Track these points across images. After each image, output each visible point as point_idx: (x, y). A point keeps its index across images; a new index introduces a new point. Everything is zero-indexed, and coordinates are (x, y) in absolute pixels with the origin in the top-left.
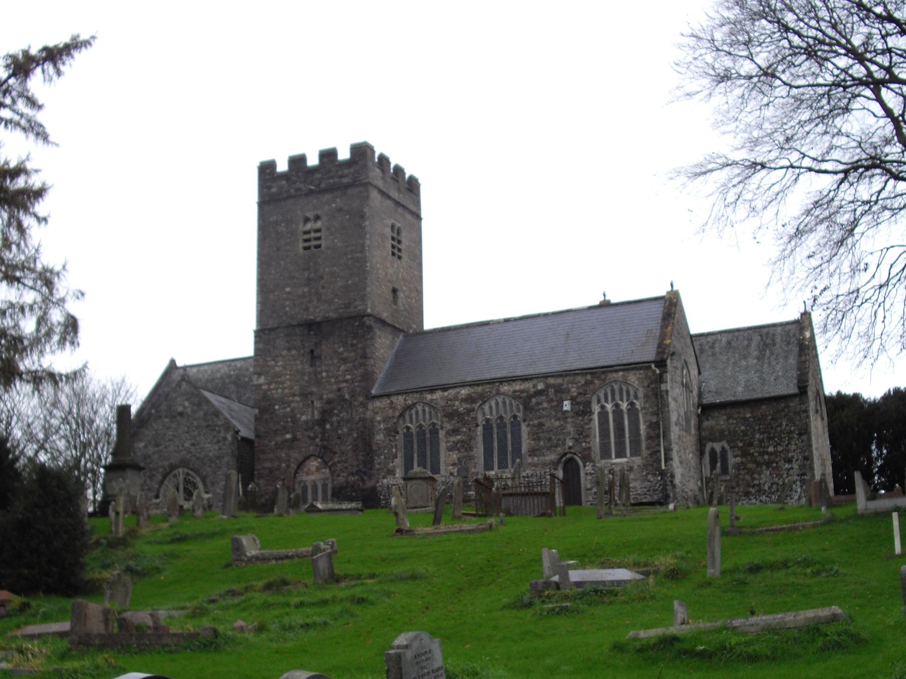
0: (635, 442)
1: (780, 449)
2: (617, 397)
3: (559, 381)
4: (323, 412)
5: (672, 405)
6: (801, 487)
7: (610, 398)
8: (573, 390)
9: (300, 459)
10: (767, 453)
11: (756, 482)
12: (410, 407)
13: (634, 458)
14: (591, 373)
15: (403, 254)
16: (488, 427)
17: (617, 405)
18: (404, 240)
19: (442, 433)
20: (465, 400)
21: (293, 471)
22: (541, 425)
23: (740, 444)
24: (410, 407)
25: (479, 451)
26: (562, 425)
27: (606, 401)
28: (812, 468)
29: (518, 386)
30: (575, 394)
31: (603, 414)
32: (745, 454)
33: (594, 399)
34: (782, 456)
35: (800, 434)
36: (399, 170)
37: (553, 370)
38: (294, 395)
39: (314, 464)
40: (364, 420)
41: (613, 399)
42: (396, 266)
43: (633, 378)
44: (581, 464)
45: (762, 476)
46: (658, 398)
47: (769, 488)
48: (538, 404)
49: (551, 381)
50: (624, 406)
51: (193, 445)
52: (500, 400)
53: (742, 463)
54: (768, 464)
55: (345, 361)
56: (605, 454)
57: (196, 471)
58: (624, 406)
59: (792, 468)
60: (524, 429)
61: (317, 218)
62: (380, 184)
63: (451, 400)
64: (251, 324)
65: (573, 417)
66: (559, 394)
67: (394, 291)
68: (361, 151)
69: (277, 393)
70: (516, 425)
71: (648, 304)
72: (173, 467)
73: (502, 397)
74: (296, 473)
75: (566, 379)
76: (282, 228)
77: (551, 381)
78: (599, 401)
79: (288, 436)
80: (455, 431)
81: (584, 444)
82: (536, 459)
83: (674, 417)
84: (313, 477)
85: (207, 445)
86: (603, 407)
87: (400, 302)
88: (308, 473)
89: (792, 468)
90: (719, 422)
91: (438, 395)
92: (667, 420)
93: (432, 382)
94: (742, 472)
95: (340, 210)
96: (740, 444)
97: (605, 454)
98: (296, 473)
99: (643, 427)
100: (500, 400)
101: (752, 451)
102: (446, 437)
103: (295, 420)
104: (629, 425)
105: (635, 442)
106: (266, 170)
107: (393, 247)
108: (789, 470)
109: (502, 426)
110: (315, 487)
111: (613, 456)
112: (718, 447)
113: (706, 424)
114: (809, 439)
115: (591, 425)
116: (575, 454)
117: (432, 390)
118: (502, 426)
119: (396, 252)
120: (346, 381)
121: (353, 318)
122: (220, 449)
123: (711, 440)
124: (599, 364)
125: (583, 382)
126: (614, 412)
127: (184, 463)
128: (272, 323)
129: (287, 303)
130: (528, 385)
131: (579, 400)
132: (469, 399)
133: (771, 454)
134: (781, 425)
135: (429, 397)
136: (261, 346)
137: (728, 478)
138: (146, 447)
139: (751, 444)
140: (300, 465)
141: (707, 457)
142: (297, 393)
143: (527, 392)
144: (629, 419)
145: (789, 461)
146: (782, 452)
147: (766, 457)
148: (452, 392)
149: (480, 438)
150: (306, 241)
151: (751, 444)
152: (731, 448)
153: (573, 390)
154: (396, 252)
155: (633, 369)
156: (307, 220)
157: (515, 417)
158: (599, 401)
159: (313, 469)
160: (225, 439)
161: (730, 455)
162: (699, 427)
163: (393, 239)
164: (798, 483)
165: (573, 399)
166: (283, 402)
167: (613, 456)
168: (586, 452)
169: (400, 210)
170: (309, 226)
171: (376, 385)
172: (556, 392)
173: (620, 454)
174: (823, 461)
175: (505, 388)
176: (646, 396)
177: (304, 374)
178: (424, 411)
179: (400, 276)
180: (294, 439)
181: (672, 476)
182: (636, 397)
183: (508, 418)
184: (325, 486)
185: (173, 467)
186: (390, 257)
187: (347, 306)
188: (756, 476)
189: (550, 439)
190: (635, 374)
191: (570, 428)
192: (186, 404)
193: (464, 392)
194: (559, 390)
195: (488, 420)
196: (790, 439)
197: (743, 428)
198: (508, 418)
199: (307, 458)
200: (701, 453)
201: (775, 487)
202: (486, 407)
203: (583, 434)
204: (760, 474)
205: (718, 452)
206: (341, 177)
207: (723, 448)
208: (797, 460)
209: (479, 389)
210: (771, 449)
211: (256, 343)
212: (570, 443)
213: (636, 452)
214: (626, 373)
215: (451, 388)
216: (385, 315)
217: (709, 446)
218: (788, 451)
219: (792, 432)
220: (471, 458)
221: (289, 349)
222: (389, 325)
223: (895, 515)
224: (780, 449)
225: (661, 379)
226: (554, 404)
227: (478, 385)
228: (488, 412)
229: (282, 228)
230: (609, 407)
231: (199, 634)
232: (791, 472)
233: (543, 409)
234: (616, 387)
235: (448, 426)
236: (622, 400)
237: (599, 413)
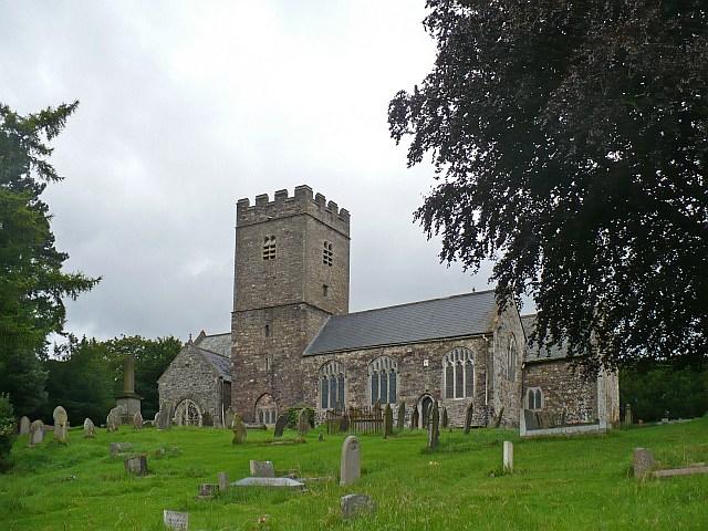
0: (470, 387)
3: (422, 346)
4: (273, 366)
5: (496, 362)
16: (375, 377)
17: (459, 363)
22: (409, 375)
24: (327, 363)
29: (395, 350)
31: (450, 369)
32: (553, 395)
36: (333, 205)
39: (267, 398)
43: (470, 344)
46: (486, 357)
50: (463, 363)
52: (383, 358)
55: (287, 332)
56: (450, 394)
57: (197, 402)
58: (463, 363)
61: (273, 238)
62: (316, 215)
64: (229, 306)
67: (325, 287)
68: (303, 191)
69: (245, 354)
70: (393, 375)
71: (464, 299)
72: (183, 399)
76: (250, 245)
77: (417, 346)
80: (354, 379)
83: (497, 371)
86: (450, 364)
87: (329, 295)
90: (537, 373)
91: (344, 355)
92: (491, 375)
93: (334, 347)
95: (287, 233)
97: (450, 394)
100: (383, 358)
103: (256, 371)
105: (470, 387)
106: (242, 205)
107: (325, 257)
110: (268, 414)
112: (534, 390)
114: (596, 385)
117: (341, 352)
119: (328, 261)
123: (530, 386)
127: (190, 397)
130: (402, 350)
132: (364, 358)
141: (527, 397)
148: (353, 353)
149: (370, 384)
150: (265, 253)
154: (328, 261)
156: (267, 239)
162: (523, 377)
165: (430, 359)
169: (332, 232)
170: (269, 243)
171: (307, 349)
174: (609, 400)
176: (478, 356)
180: (255, 383)
181: (493, 410)
183: (388, 371)
184: (274, 413)
185: (183, 399)
187: (290, 296)
194: (422, 353)
198: (388, 371)
202: (374, 363)
203: (436, 382)
209: (371, 351)
210: (570, 391)
212: (427, 387)
213: (470, 393)
216: (316, 303)
220: (364, 397)
223: (252, 471)
225: (489, 345)
228: (375, 367)
229: (250, 245)
231: (273, 503)
234: (459, 351)
235: (350, 376)
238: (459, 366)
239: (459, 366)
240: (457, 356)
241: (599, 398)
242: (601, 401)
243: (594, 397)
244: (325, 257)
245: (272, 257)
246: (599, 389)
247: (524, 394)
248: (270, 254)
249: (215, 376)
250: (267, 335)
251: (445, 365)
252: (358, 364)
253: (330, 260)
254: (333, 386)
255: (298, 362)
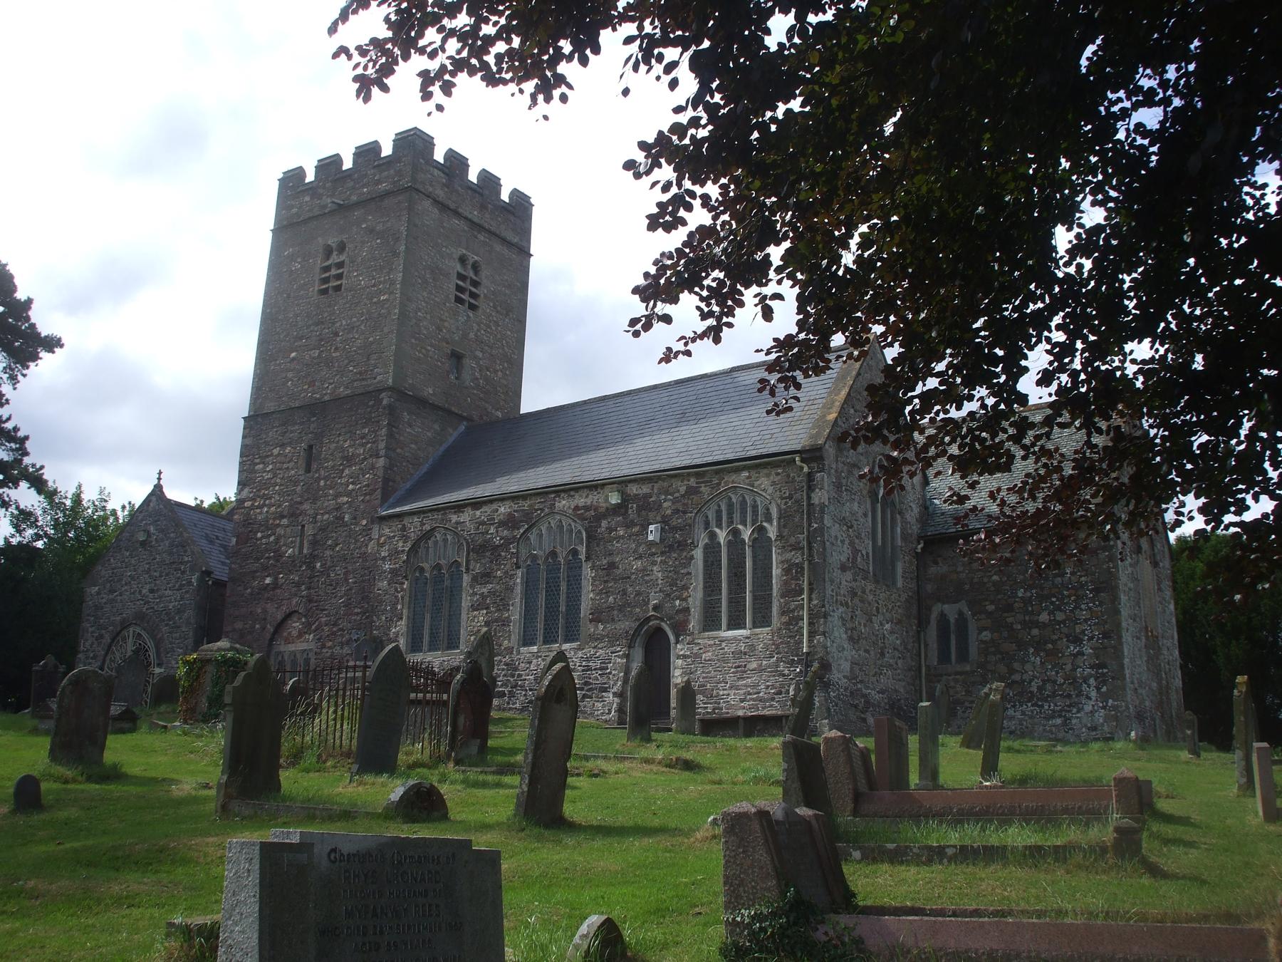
1: (1060, 616)
2: (737, 516)
3: (645, 489)
4: (314, 543)
6: (1098, 689)
7: (749, 520)
8: (665, 505)
9: (280, 617)
10: (1036, 624)
11: (1017, 677)
12: (427, 535)
13: (758, 630)
14: (697, 475)
15: (480, 303)
17: (736, 533)
18: (485, 282)
19: (466, 579)
20: (502, 524)
21: (268, 636)
23: (991, 608)
25: (515, 613)
26: (644, 569)
27: (720, 526)
28: (1118, 655)
30: (669, 512)
31: (712, 549)
33: (700, 519)
34: (1065, 630)
35: (1097, 591)
37: (637, 471)
38: (282, 517)
39: (296, 625)
40: (364, 556)
41: (730, 522)
42: (462, 319)
43: (765, 483)
44: (672, 638)
45: (1028, 667)
47: (1040, 689)
48: (610, 530)
49: (633, 489)
50: (746, 534)
51: (152, 591)
53: (992, 640)
54: (1039, 645)
58: (746, 534)
59: (1081, 653)
60: (588, 572)
63: (483, 523)
64: (242, 405)
65: (663, 553)
66: (643, 513)
67: (457, 357)
72: (125, 625)
73: (558, 517)
74: (272, 640)
75: (656, 486)
77: (633, 489)
78: (707, 524)
79: (268, 581)
80: (486, 577)
81: (677, 602)
82: (601, 627)
84: (292, 648)
85: (168, 592)
86: (713, 536)
87: (466, 376)
88: (288, 641)
89: (1081, 653)
91: (466, 516)
94: (992, 658)
96: (991, 608)
98: (272, 640)
99: (776, 572)
101: (1010, 620)
102: (472, 587)
103: (279, 556)
104: (754, 569)
107: (459, 288)
108: (1075, 656)
109: (553, 569)
111: (724, 626)
112: (951, 610)
113: (933, 570)
115: (692, 569)
116: (662, 620)
118: (553, 569)
120: (349, 494)
121: (367, 394)
122: (182, 598)
124: (710, 459)
125: (683, 490)
126: (730, 544)
127: (140, 617)
128: (270, 406)
129: (290, 375)
131: (674, 522)
132: (510, 522)
133: (1044, 625)
134: (1063, 575)
135: (454, 518)
136: (248, 441)
137: (968, 668)
138: (98, 593)
139: (1009, 608)
140: (280, 626)
141: (932, 632)
142: (285, 513)
143: (596, 509)
144: (754, 557)
145: (1077, 640)
146: (1063, 622)
147: (1035, 632)
148: (487, 509)
151: (1009, 608)
152: (973, 615)
153: (665, 505)
155: (765, 465)
157: (575, 553)
158: (707, 524)
159: (295, 633)
160: (190, 583)
161: (972, 626)
163: (461, 277)
164: (1092, 681)
165: (665, 521)
166: (266, 526)
167: (724, 626)
168: (681, 617)
170: (335, 258)
172: (640, 509)
173: (736, 623)
175: (563, 503)
177: (296, 483)
178: (445, 540)
179: (472, 335)
180: (275, 586)
182: (769, 519)
185: (125, 625)
186: (451, 303)
188: (1016, 665)
189: (624, 592)
190: (768, 476)
191: (658, 573)
192: (152, 529)
193: (503, 509)
195: (534, 558)
196: (1079, 598)
197: (995, 578)
199: (288, 616)
200: (922, 623)
201: (1048, 686)
203: (677, 584)
204: (1024, 662)
205: (952, 620)
206: (379, 182)
207: (961, 613)
208: (1091, 639)
209: (526, 505)
210: (1044, 617)
211: (244, 437)
213: (762, 619)
214: (753, 473)
215: (485, 503)
217: (937, 609)
218: (1076, 621)
219: (1082, 586)
221: (283, 446)
222: (434, 407)
224: (1060, 616)
226: (635, 529)
227: (524, 497)
228: (541, 542)
230: (722, 536)
232: (1080, 661)
233: (618, 538)
235: (478, 568)
236: (744, 523)
237: (706, 547)
238: (735, 540)
239: (735, 540)
240: (730, 515)
241: (1127, 637)
242: (1131, 645)
243: (1111, 633)
244: (459, 288)
245: (338, 288)
246: (1125, 613)
247: (922, 623)
248: (334, 272)
249: (193, 570)
250: (308, 470)
251: (703, 539)
252: (496, 535)
253: (473, 295)
254: (552, 590)
255: (367, 531)
